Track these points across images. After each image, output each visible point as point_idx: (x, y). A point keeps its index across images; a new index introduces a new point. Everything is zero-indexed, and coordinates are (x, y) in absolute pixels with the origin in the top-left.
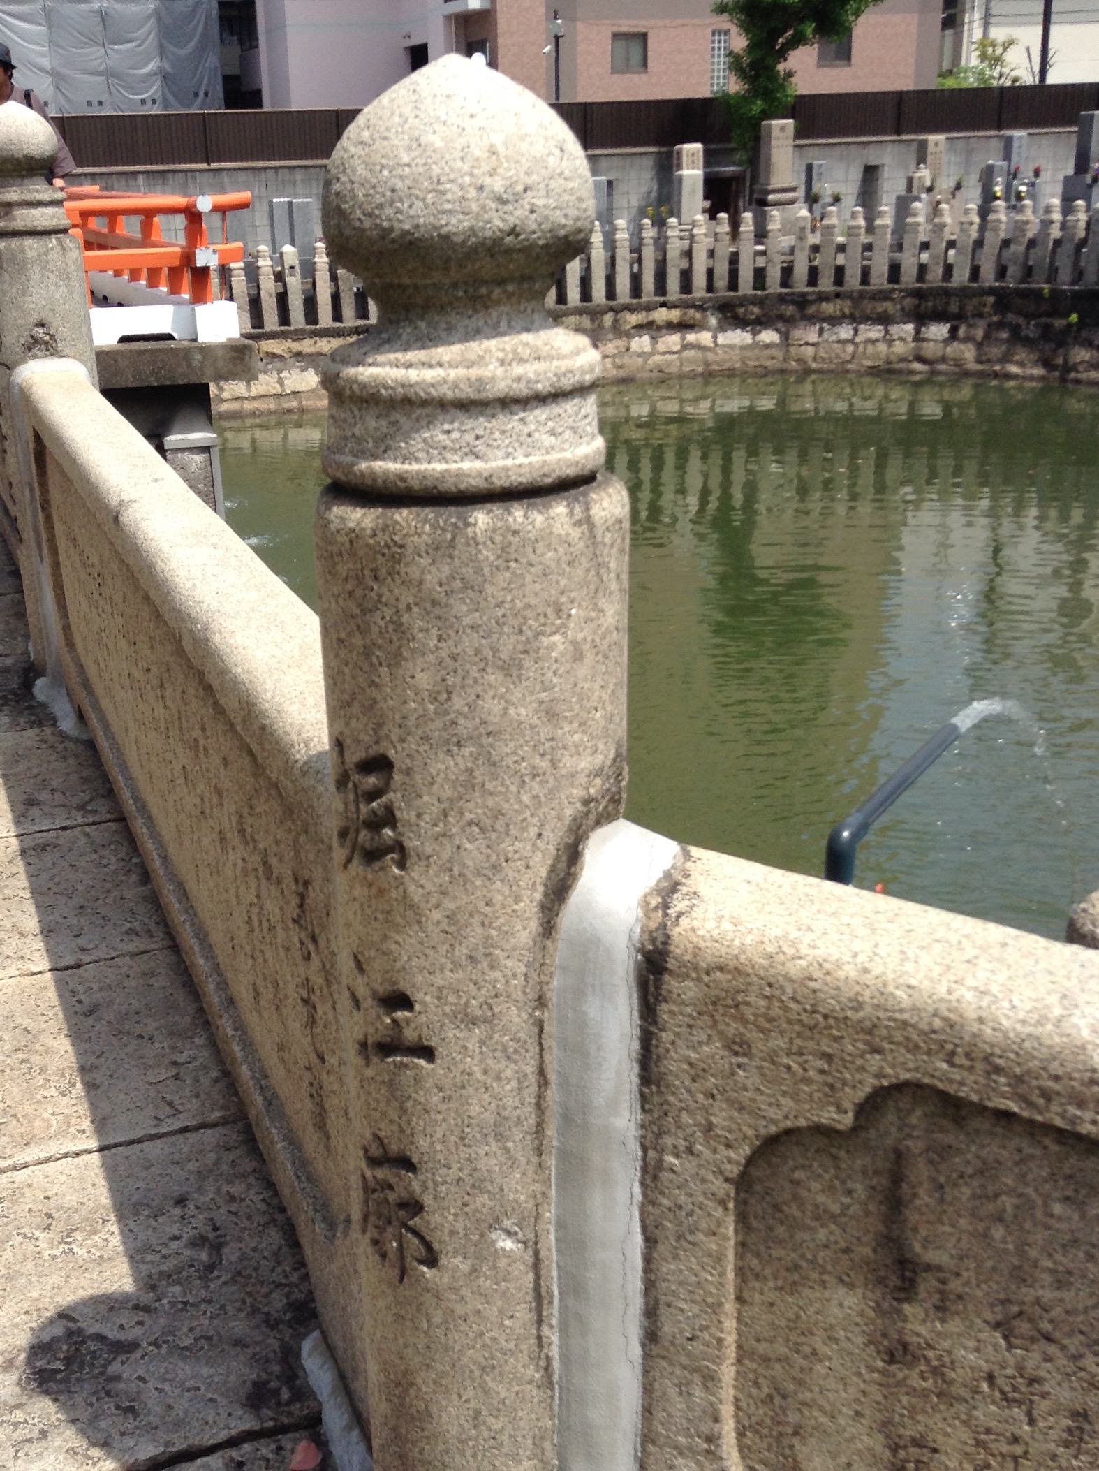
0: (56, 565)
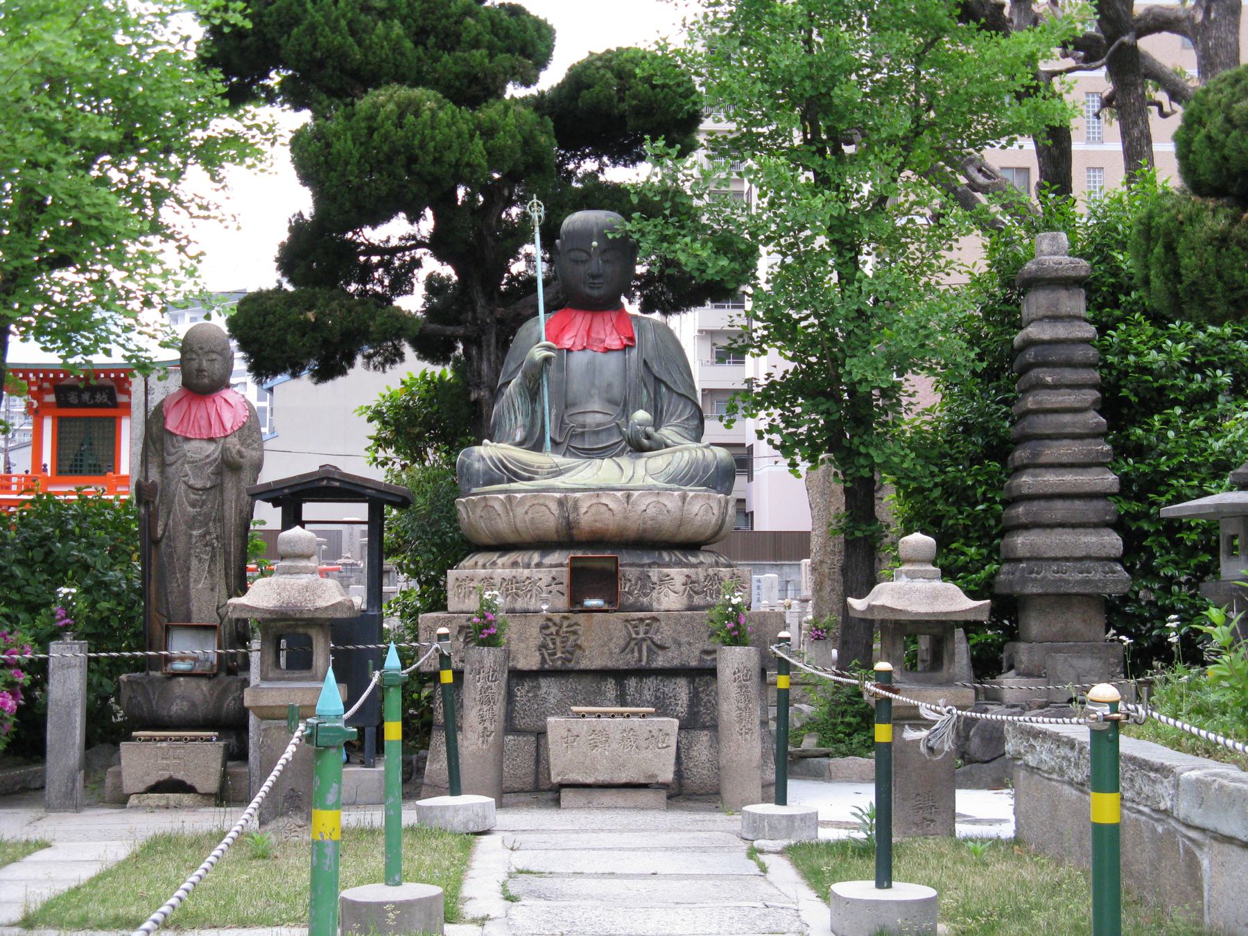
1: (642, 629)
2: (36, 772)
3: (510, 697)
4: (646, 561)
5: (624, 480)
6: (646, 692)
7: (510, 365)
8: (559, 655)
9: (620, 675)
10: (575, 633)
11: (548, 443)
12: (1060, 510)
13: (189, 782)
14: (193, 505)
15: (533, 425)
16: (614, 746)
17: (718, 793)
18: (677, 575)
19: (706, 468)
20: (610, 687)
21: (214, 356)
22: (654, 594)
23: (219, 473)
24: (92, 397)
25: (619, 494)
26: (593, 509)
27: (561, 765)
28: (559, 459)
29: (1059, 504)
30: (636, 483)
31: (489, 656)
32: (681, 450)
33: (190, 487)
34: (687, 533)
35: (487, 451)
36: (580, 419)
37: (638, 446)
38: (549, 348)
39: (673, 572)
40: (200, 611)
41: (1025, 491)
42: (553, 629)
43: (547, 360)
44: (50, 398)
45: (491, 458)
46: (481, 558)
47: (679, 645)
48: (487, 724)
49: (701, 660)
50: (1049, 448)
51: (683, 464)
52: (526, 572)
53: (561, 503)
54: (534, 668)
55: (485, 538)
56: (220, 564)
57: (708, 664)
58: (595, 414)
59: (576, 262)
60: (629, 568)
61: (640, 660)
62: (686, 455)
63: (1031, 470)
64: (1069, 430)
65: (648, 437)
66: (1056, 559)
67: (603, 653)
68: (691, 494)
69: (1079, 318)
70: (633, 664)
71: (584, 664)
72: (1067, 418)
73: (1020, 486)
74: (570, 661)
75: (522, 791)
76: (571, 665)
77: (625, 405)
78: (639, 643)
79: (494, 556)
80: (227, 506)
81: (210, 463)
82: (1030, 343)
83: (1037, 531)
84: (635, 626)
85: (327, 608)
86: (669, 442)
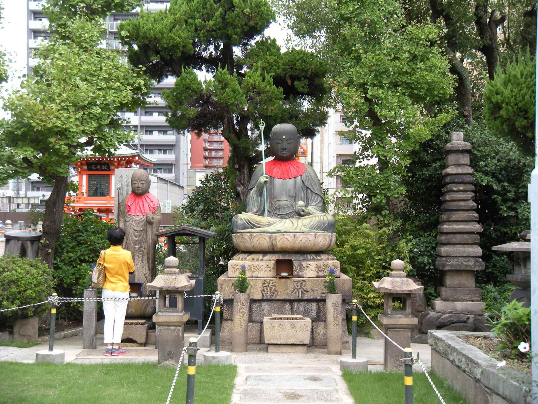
0: (397, 328)
1: (299, 285)
2: (79, 330)
3: (250, 310)
4: (301, 259)
5: (294, 228)
6: (301, 308)
7: (253, 182)
8: (269, 294)
9: (291, 301)
10: (275, 286)
11: (266, 212)
12: (458, 238)
13: (134, 339)
14: (136, 237)
15: (261, 205)
16: (288, 330)
17: (326, 345)
18: (313, 264)
19: (324, 224)
20: (288, 306)
21: (143, 182)
22: (304, 271)
23: (145, 225)
24: (101, 167)
25: (291, 234)
26: (282, 240)
27: (268, 337)
28: (270, 219)
29: (458, 236)
30: (298, 230)
31: (243, 297)
32: (315, 217)
33: (135, 230)
34: (316, 248)
35: (243, 217)
36: (278, 203)
37: (300, 214)
38: (267, 178)
39: (311, 263)
40: (138, 275)
41: (445, 231)
42: (267, 284)
43: (266, 182)
44: (85, 167)
45: (245, 219)
46: (241, 256)
47: (313, 290)
48: (242, 321)
49: (321, 296)
50: (454, 215)
51: (316, 222)
52: (257, 263)
53: (270, 238)
54: (260, 299)
55: (243, 248)
56: (146, 257)
57: (323, 298)
58: (284, 201)
59: (277, 143)
60: (296, 260)
61: (299, 296)
62: (317, 218)
63: (447, 223)
64: (462, 208)
65: (303, 211)
66: (456, 257)
67: (285, 294)
68: (318, 234)
69: (467, 165)
70: (296, 298)
71: (278, 298)
72: (461, 203)
73: (443, 229)
74: (273, 296)
75: (255, 344)
76: (273, 298)
77: (295, 198)
78: (298, 290)
79: (245, 256)
80: (148, 237)
81: (142, 221)
82: (448, 175)
83: (450, 246)
84: (297, 284)
85: (182, 287)
86: (311, 212)
